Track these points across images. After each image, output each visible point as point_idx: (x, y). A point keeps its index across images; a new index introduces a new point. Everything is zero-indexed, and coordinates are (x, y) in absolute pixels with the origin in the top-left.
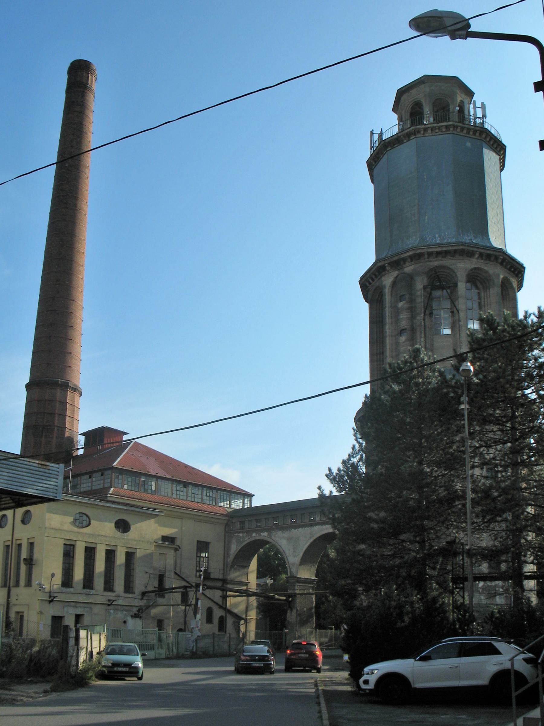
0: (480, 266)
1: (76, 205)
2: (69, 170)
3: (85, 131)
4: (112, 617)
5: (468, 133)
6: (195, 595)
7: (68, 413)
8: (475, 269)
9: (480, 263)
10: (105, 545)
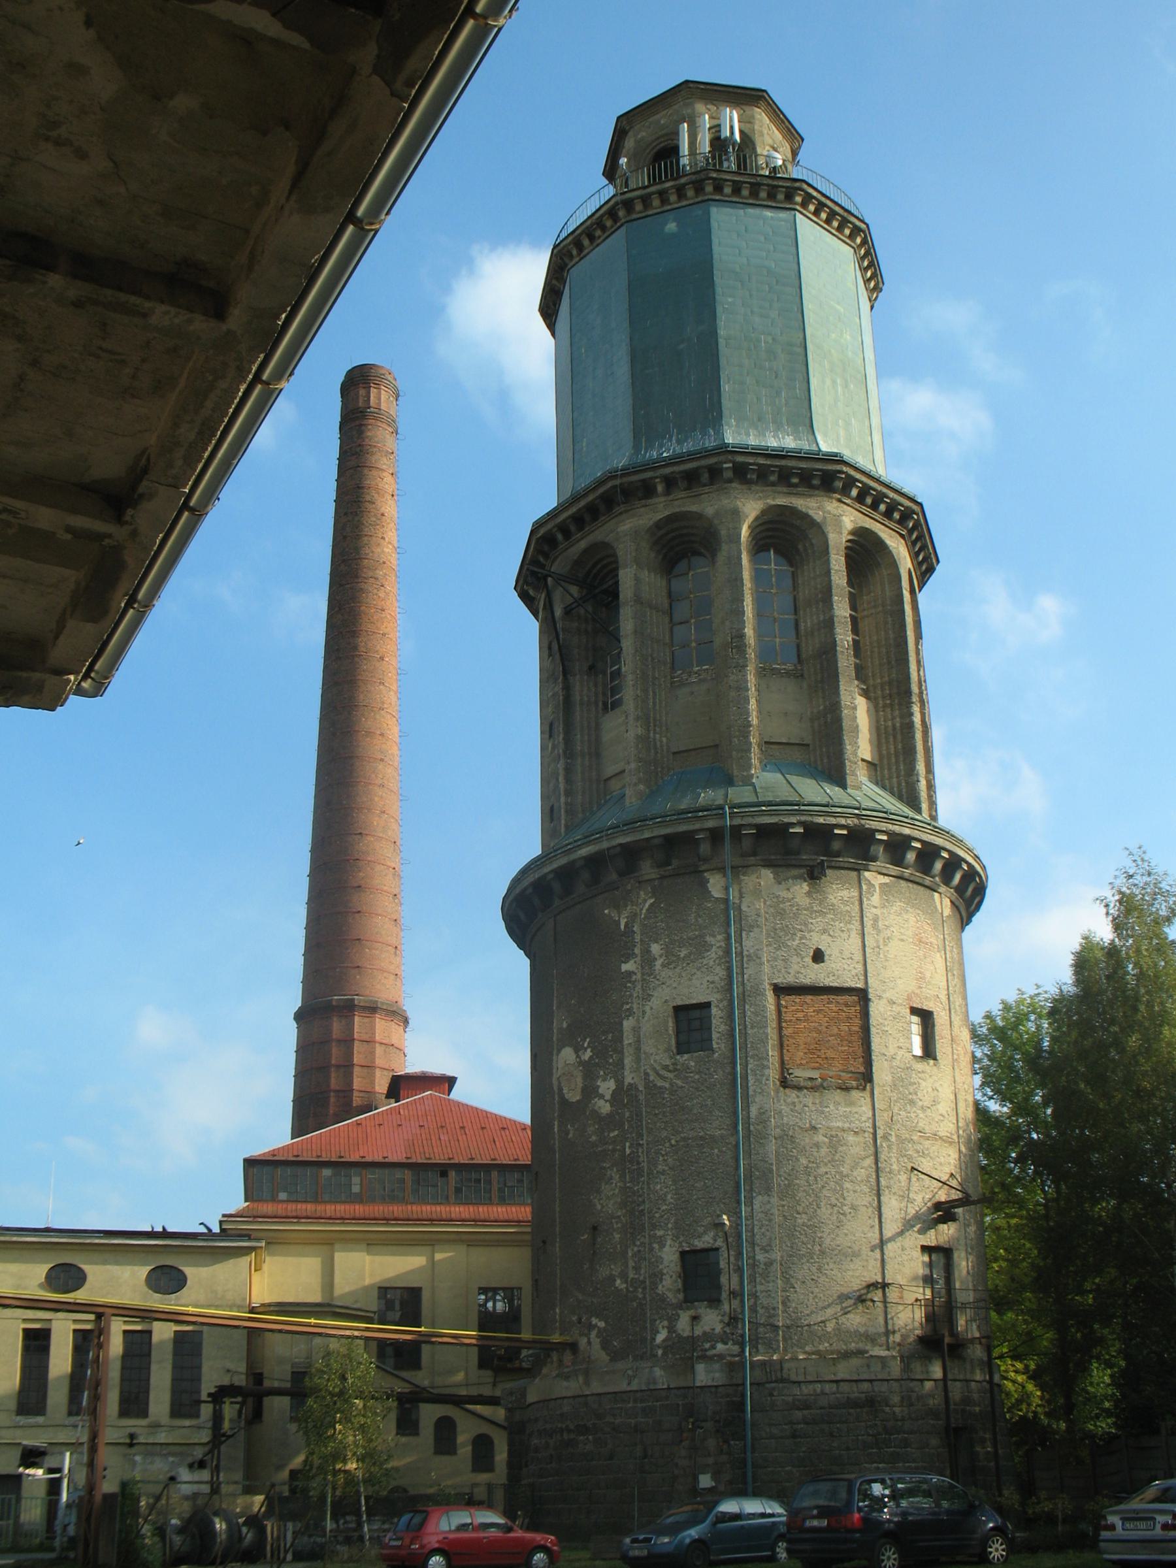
0: (678, 510)
1: (355, 648)
2: (341, 585)
3: (368, 498)
4: (138, 1468)
5: (664, 201)
6: (478, 1408)
7: (357, 1059)
8: (670, 519)
9: (676, 503)
10: (71, 1322)
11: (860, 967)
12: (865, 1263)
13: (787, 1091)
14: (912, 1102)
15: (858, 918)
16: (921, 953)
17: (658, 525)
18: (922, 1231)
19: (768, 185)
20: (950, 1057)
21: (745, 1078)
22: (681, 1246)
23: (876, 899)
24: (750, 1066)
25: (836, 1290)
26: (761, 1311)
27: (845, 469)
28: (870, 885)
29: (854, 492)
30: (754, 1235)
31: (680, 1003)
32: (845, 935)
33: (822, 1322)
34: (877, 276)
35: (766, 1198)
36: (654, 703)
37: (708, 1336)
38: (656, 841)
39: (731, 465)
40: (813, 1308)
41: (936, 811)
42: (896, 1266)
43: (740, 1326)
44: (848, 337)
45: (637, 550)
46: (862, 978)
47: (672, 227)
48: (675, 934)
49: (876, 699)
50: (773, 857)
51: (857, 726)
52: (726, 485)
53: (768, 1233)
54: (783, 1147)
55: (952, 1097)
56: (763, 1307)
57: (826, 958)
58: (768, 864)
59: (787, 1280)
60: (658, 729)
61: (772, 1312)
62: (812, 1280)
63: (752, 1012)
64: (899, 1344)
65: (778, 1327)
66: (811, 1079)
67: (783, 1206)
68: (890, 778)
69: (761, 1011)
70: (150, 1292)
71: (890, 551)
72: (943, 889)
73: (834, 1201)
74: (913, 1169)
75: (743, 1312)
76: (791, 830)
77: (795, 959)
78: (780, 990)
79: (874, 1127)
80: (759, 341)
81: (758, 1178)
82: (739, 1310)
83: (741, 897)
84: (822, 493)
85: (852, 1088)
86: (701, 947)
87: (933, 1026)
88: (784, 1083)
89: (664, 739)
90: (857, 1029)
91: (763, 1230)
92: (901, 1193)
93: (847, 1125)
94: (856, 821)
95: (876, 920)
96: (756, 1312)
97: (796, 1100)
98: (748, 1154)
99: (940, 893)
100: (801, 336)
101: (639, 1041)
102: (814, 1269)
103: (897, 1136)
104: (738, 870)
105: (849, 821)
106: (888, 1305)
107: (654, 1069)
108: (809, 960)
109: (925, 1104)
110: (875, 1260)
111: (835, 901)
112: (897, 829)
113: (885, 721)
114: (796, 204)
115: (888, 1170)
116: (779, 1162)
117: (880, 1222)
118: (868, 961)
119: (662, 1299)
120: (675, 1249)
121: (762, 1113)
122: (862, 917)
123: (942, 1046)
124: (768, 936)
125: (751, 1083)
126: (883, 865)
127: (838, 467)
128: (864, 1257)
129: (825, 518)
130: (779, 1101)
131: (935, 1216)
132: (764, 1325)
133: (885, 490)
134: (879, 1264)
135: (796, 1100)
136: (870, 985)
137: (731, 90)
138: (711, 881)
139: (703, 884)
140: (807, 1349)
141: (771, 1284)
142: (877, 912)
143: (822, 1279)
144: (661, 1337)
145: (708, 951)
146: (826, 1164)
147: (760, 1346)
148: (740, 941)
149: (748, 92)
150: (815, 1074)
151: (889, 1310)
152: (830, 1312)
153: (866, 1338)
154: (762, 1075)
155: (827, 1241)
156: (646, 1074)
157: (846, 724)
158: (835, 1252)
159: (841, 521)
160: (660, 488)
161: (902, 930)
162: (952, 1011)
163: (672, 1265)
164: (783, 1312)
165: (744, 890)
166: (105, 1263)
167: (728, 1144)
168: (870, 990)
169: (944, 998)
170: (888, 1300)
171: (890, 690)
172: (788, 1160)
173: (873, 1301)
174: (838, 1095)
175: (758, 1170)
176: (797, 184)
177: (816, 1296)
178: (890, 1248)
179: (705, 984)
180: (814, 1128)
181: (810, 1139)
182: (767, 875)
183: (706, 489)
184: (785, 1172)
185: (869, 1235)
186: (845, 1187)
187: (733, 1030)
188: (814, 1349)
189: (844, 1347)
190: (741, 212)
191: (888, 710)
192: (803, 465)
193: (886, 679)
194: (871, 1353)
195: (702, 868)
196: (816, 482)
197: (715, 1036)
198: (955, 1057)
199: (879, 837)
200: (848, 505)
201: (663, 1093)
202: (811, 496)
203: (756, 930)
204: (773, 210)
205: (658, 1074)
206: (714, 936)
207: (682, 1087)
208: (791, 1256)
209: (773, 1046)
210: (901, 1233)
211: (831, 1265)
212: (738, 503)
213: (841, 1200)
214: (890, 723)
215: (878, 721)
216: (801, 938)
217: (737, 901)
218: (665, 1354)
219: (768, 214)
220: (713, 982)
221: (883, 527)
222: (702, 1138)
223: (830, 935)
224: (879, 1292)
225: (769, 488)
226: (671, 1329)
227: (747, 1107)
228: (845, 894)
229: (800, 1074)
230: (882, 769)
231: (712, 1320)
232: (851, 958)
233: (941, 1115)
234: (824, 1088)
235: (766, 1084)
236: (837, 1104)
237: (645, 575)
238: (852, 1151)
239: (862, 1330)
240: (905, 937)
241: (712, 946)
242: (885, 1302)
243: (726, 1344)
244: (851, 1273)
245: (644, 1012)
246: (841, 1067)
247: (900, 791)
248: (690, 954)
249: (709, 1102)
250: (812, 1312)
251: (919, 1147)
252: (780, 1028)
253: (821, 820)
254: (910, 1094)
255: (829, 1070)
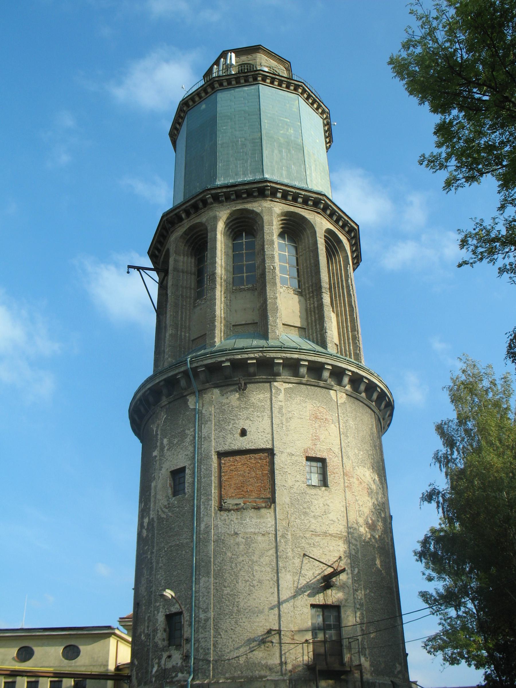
8: (191, 229)
9: (191, 221)
11: (270, 436)
12: (267, 617)
13: (222, 513)
14: (305, 513)
15: (269, 409)
16: (317, 425)
17: (186, 233)
18: (312, 595)
19: (243, 76)
20: (342, 485)
21: (199, 508)
22: (166, 612)
23: (281, 397)
24: (202, 500)
25: (247, 636)
26: (201, 651)
27: (269, 184)
28: (277, 389)
29: (279, 195)
30: (199, 602)
31: (173, 469)
32: (260, 419)
33: (237, 657)
34: (321, 106)
35: (207, 579)
36: (182, 318)
37: (174, 669)
38: (162, 383)
39: (210, 196)
40: (232, 648)
41: (360, 350)
42: (289, 618)
43: (190, 661)
44: (292, 131)
45: (176, 247)
46: (271, 442)
47: (204, 106)
48: (173, 432)
49: (305, 295)
50: (218, 382)
51: (277, 307)
52: (211, 206)
53: (207, 601)
54: (218, 547)
55: (344, 509)
56: (202, 648)
57: (248, 433)
58: (217, 386)
59: (216, 630)
60: (183, 330)
61: (207, 651)
62: (232, 629)
63: (205, 469)
64: (290, 671)
65: (210, 661)
66: (237, 504)
67: (216, 583)
68: (312, 334)
69: (209, 469)
70: (63, 659)
71: (309, 221)
72: (337, 387)
73: (247, 578)
74: (305, 555)
75: (191, 653)
76: (223, 365)
77: (229, 436)
78: (221, 455)
79: (276, 530)
80: (238, 141)
81: (203, 567)
82: (190, 650)
83: (203, 406)
84: (261, 199)
85: (263, 508)
86: (183, 435)
87: (327, 467)
88: (221, 508)
89: (187, 335)
90: (266, 472)
91: (204, 599)
92: (295, 571)
93: (257, 531)
94: (260, 354)
95: (281, 408)
96: (198, 651)
97: (227, 518)
98: (198, 552)
99: (336, 391)
100: (259, 134)
101: (156, 493)
102: (233, 622)
103: (292, 535)
104: (201, 392)
105: (256, 355)
106: (282, 645)
107: (161, 508)
108: (237, 436)
109: (317, 514)
110: (274, 615)
111: (255, 401)
112: (289, 355)
113: (310, 305)
114: (260, 81)
115: (285, 556)
116: (215, 556)
117: (278, 590)
118: (275, 432)
119: (156, 645)
120: (163, 614)
121: (208, 527)
122: (271, 408)
123: (330, 479)
124: (215, 425)
125: (202, 510)
126: (285, 377)
127: (265, 184)
128: (266, 613)
129: (262, 210)
130: (217, 519)
131: (323, 584)
132: (203, 660)
133: (298, 191)
134: (277, 618)
135: (227, 518)
136: (275, 446)
137: (244, 49)
138: (190, 400)
139: (186, 402)
140: (227, 675)
141: (207, 633)
142: (283, 404)
143: (238, 629)
144: (155, 670)
145: (186, 438)
146: (243, 555)
147: (199, 674)
148: (200, 430)
149: (253, 48)
150: (241, 502)
151: (283, 648)
152: (242, 650)
153: (266, 667)
154: (208, 505)
155: (242, 605)
156: (158, 511)
157: (269, 307)
158: (247, 611)
159: (272, 210)
160: (183, 216)
161: (301, 413)
162: (344, 458)
163: (162, 623)
164: (213, 651)
165: (204, 402)
166: (42, 646)
167: (189, 547)
168: (275, 449)
169: (337, 450)
170: (283, 641)
171: (312, 289)
172: (220, 554)
173: (272, 642)
174: (252, 513)
175: (203, 561)
176: (257, 72)
177: (234, 640)
178: (284, 607)
179: (184, 456)
180: (236, 534)
181: (234, 541)
182: (217, 391)
183: (203, 210)
184: (218, 562)
185: (271, 599)
186: (254, 569)
187: (194, 481)
188: (231, 675)
189: (251, 674)
190: (233, 91)
191: (312, 299)
192: (247, 187)
193: (310, 284)
194: (269, 678)
195: (185, 394)
196: (256, 194)
197: (187, 485)
198: (346, 484)
199: (277, 361)
200: (278, 202)
201: (163, 521)
202: (255, 201)
203: (209, 423)
204: (248, 87)
205: (162, 511)
206: (189, 430)
207: (172, 516)
208: (220, 614)
209: (215, 487)
210: (294, 597)
211: (244, 620)
212: (217, 213)
213: (252, 577)
214: (312, 306)
215: (306, 306)
216: (233, 424)
217: (201, 409)
218: (155, 681)
219: (246, 88)
220: (187, 455)
221: (304, 210)
222: (178, 545)
223: (250, 420)
224: (277, 636)
225: (232, 203)
226: (159, 666)
227: (198, 525)
228: (261, 396)
229: (230, 502)
230: (308, 330)
231: (177, 658)
232: (264, 432)
233: (332, 520)
234: (244, 509)
235: (210, 510)
236: (251, 517)
237: (181, 258)
238: (260, 546)
239: (263, 662)
240: (303, 417)
241: (188, 435)
242: (280, 643)
243: (183, 673)
244: (256, 624)
245: (159, 477)
246: (256, 496)
247: (317, 340)
248: (178, 441)
249: (182, 524)
250: (231, 651)
251: (310, 541)
252: (220, 477)
253: (239, 357)
254: (305, 508)
255: (249, 498)
